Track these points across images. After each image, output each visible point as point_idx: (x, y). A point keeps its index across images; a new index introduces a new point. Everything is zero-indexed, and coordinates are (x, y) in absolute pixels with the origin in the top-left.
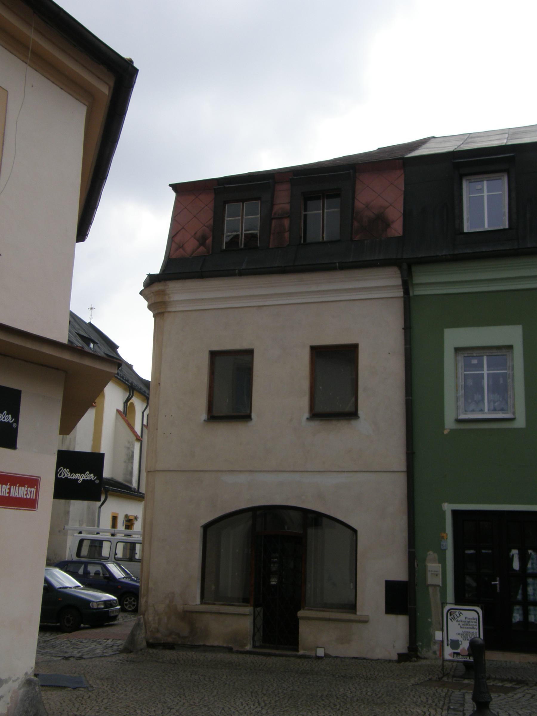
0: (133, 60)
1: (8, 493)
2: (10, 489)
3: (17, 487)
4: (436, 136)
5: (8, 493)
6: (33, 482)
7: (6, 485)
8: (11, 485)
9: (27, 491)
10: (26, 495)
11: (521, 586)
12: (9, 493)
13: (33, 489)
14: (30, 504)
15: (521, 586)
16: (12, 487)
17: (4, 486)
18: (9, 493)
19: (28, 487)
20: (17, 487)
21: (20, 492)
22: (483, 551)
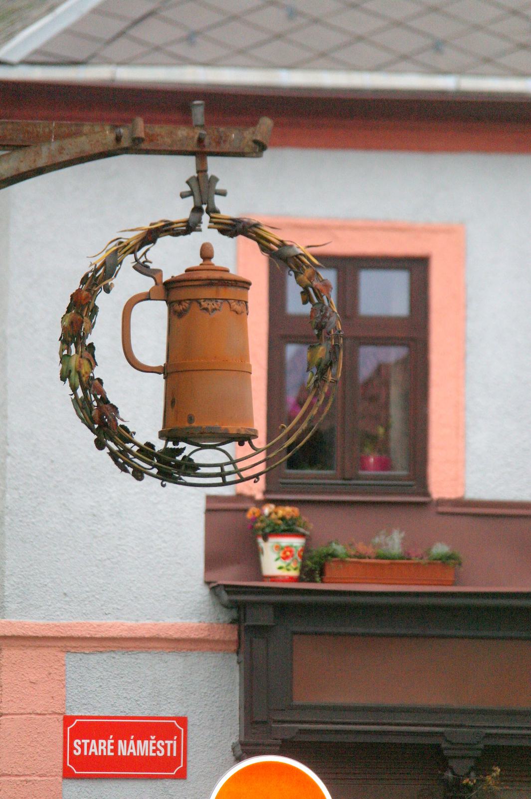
0: (149, 441)
1: (112, 751)
2: (115, 745)
3: (132, 742)
4: (96, 358)
5: (112, 751)
6: (171, 729)
7: (107, 739)
8: (116, 740)
9: (154, 745)
10: (154, 751)
11: (126, 466)
12: (115, 750)
13: (169, 742)
14: (171, 767)
15: (126, 466)
16: (120, 742)
17: (146, 742)
18: (115, 750)
19: (157, 739)
20: (132, 742)
21: (101, 747)
22: (88, 391)
